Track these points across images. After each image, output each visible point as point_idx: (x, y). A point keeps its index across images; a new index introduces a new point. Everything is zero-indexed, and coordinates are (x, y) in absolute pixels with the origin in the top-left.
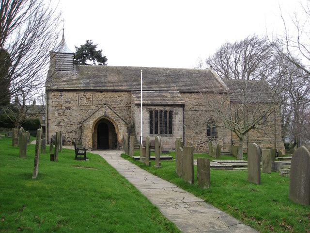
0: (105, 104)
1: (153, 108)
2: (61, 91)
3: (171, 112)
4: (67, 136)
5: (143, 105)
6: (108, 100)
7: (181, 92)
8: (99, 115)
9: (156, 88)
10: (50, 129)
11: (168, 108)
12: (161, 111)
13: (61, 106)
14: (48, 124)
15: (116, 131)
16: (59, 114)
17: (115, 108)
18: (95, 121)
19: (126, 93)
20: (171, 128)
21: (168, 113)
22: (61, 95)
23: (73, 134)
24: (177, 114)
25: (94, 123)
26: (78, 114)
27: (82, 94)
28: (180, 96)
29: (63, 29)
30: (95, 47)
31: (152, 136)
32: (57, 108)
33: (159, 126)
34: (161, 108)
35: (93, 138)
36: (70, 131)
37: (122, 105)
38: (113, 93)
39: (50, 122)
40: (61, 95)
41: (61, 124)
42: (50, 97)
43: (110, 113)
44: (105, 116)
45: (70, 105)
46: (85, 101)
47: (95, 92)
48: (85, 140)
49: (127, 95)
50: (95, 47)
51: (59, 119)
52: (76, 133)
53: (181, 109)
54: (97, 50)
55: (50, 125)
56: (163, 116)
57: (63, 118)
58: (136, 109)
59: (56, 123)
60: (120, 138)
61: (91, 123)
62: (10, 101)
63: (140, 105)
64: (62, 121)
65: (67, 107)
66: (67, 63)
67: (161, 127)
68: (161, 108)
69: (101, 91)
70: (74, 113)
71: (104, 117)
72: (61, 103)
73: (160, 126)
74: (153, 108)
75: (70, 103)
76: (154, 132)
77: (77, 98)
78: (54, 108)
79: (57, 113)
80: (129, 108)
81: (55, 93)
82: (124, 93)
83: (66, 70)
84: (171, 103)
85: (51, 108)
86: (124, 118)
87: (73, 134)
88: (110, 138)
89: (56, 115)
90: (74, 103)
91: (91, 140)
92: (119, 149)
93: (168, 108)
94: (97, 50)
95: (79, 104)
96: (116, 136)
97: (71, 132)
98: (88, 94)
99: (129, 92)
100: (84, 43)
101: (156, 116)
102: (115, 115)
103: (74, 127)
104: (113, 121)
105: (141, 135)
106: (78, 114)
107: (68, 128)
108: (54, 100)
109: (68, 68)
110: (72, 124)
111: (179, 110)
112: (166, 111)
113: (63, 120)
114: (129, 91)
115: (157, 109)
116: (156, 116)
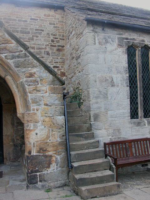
15: (20, 110)
19: (52, 12)
31: (139, 124)
76: (140, 112)
88: (8, 131)
99: (59, 11)
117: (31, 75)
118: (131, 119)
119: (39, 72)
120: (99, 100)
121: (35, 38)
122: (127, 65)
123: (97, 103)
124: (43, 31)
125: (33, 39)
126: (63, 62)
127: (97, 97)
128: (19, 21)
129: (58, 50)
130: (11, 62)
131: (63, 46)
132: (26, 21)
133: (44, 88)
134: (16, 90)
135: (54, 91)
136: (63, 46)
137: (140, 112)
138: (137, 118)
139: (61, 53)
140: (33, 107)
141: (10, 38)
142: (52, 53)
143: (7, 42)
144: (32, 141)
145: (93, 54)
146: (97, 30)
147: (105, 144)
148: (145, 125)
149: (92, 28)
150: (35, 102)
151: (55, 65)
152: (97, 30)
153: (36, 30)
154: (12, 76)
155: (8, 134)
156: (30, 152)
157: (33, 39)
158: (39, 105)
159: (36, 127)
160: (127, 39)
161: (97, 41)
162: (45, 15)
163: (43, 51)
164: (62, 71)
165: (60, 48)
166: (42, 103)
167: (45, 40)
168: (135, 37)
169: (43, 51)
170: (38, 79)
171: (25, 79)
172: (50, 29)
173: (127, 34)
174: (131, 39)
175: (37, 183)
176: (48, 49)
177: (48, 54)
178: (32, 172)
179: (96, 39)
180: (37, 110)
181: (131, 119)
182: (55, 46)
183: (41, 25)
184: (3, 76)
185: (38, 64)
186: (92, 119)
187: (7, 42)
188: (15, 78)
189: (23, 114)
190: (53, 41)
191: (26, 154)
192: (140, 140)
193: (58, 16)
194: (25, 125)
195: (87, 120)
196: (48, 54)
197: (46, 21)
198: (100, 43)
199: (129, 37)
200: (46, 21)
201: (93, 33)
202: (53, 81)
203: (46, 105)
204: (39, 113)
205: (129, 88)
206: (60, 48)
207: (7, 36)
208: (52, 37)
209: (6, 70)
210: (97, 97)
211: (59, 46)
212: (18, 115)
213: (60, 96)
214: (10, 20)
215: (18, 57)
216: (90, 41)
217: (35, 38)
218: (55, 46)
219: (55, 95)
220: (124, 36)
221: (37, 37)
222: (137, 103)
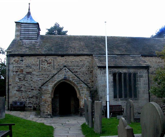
0: (65, 66)
1: (116, 70)
2: (22, 56)
3: (135, 74)
4: (28, 102)
5: (109, 67)
6: (69, 64)
7: (142, 56)
8: (60, 77)
9: (118, 53)
10: (10, 95)
11: (132, 71)
12: (125, 74)
13: (22, 71)
14: (9, 89)
15: (78, 96)
16: (19, 79)
17: (77, 72)
18: (55, 85)
19: (88, 57)
20: (135, 88)
21: (132, 75)
22: (22, 60)
23: (34, 100)
24: (141, 76)
25: (53, 88)
26: (39, 79)
27: (43, 58)
28: (143, 59)
29: (29, 4)
30: (62, 29)
31: (117, 100)
32: (18, 73)
33: (123, 89)
34: (124, 71)
35: (52, 104)
36: (31, 96)
37: (84, 69)
38: (75, 57)
39: (10, 87)
40: (22, 60)
41: (22, 89)
42: (11, 62)
43: (70, 75)
44: (65, 79)
45: (31, 70)
46: (46, 66)
47: (56, 57)
48: (44, 105)
49: (88, 59)
50: (62, 29)
51: (19, 84)
52: (37, 98)
53: (146, 71)
54: (64, 30)
55: (10, 90)
56: (127, 79)
57: (24, 83)
58: (98, 71)
59: (16, 89)
60: (82, 103)
61: (50, 87)
62: (3, 79)
63: (105, 67)
64: (23, 86)
65: (28, 72)
66: (31, 33)
67: (125, 90)
68: (124, 71)
69: (62, 56)
70: (35, 78)
71: (64, 81)
72: (22, 68)
73: (125, 90)
74: (116, 70)
75: (31, 68)
76: (118, 96)
77: (38, 63)
78: (15, 73)
79: (17, 78)
80: (91, 72)
81: (16, 58)
82: (86, 57)
83: (30, 38)
84: (135, 65)
85: (12, 73)
86: (86, 83)
87: (34, 100)
88: (72, 103)
89: (17, 80)
90: (35, 68)
91: (50, 106)
92: (81, 115)
93: (132, 71)
94: (64, 30)
95: (39, 68)
96: (77, 101)
97: (32, 97)
98: (50, 59)
99: (91, 56)
100: (53, 25)
101: (120, 79)
102: (76, 78)
103: (35, 92)
104: (75, 84)
105: (108, 100)
106: (39, 79)
107: (29, 93)
108: (14, 65)
109: (33, 37)
110: (33, 90)
111: (144, 73)
112: (130, 74)
113: (24, 85)
114: (92, 55)
115: (120, 71)
116: (120, 79)
117: (81, 86)
118: (114, 98)
119: (83, 85)
120: (102, 92)
121: (82, 68)
122: (113, 80)
123: (102, 93)
124: (85, 65)
125: (81, 69)
126: (93, 77)
127: (101, 92)
128: (76, 62)
129: (91, 72)
130: (76, 83)
131: (93, 71)
132: (78, 62)
133: (85, 90)
134: (77, 90)
135: (87, 90)
136: (93, 71)
137: (118, 96)
138: (117, 98)
139: (92, 73)
140: (82, 95)
141: (75, 76)
142: (88, 73)
143: (74, 77)
144: (81, 104)
145: (100, 78)
146: (101, 69)
147: (104, 106)
148: (119, 100)
149: (100, 69)
150: (82, 93)
151: (89, 78)
152: (101, 69)
153: (82, 65)
154: (76, 86)
155: (73, 104)
156: (81, 107)
157: (81, 69)
158: (83, 94)
159: (82, 100)
160: (113, 71)
161: (102, 73)
162: (85, 59)
163: (85, 73)
164: (92, 80)
165: (91, 71)
166: (84, 94)
167: (85, 69)
168: (116, 70)
169: (85, 73)
170: (83, 87)
171: (79, 87)
172: (88, 64)
173: (112, 69)
174: (114, 71)
175: (83, 115)
176: (87, 72)
177: (87, 74)
178: (81, 112)
179: (101, 72)
180: (83, 96)
181: (114, 98)
182: (89, 71)
183: (84, 63)
184: (73, 86)
185: (83, 83)
186: (100, 99)
187: (74, 77)
188: (77, 87)
189: (79, 97)
190: (88, 69)
191: (80, 107)
192: (117, 105)
193: (90, 58)
194: (79, 100)
195: (136, 113)
196: (87, 74)
197: (86, 61)
198: (103, 74)
199: (113, 70)
200: (86, 61)
201: (100, 71)
202: (87, 87)
203: (85, 94)
204: (83, 97)
205: (113, 88)
206: (91, 71)
207: (74, 76)
208: (88, 67)
209: (74, 85)
210: (101, 92)
211: (91, 71)
212: (78, 97)
213: (89, 92)
214: (72, 62)
215: (78, 81)
216: (99, 73)
217: (82, 68)
218: (89, 71)
219: (88, 91)
220: (112, 70)
221: (82, 68)
222: (117, 93)
